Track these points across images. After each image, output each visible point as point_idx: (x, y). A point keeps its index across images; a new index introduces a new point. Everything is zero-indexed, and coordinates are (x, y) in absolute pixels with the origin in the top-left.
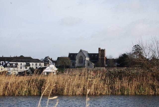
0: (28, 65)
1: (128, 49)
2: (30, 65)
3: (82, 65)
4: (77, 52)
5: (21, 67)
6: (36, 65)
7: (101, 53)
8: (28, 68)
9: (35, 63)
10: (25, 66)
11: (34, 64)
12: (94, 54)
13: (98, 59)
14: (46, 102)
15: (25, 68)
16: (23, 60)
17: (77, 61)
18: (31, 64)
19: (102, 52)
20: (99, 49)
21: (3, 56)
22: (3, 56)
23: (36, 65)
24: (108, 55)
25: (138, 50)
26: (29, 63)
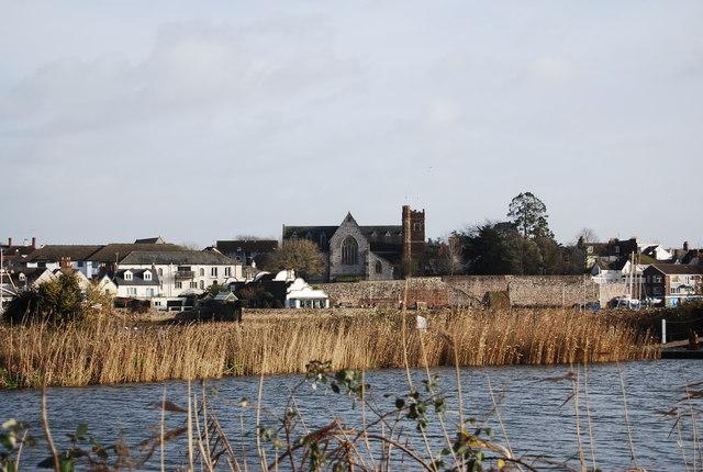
0: (184, 273)
1: (497, 211)
2: (192, 275)
3: (356, 269)
4: (337, 223)
5: (607, 287)
6: (215, 272)
7: (412, 226)
8: (186, 284)
9: (211, 267)
10: (176, 278)
11: (208, 269)
12: (382, 230)
13: (400, 248)
14: (185, 440)
15: (173, 286)
16: (164, 255)
17: (336, 256)
18: (194, 268)
19: (416, 219)
20: (405, 209)
21: (685, 245)
22: (685, 245)
23: (215, 272)
24: (435, 231)
25: (529, 208)
26: (189, 269)
